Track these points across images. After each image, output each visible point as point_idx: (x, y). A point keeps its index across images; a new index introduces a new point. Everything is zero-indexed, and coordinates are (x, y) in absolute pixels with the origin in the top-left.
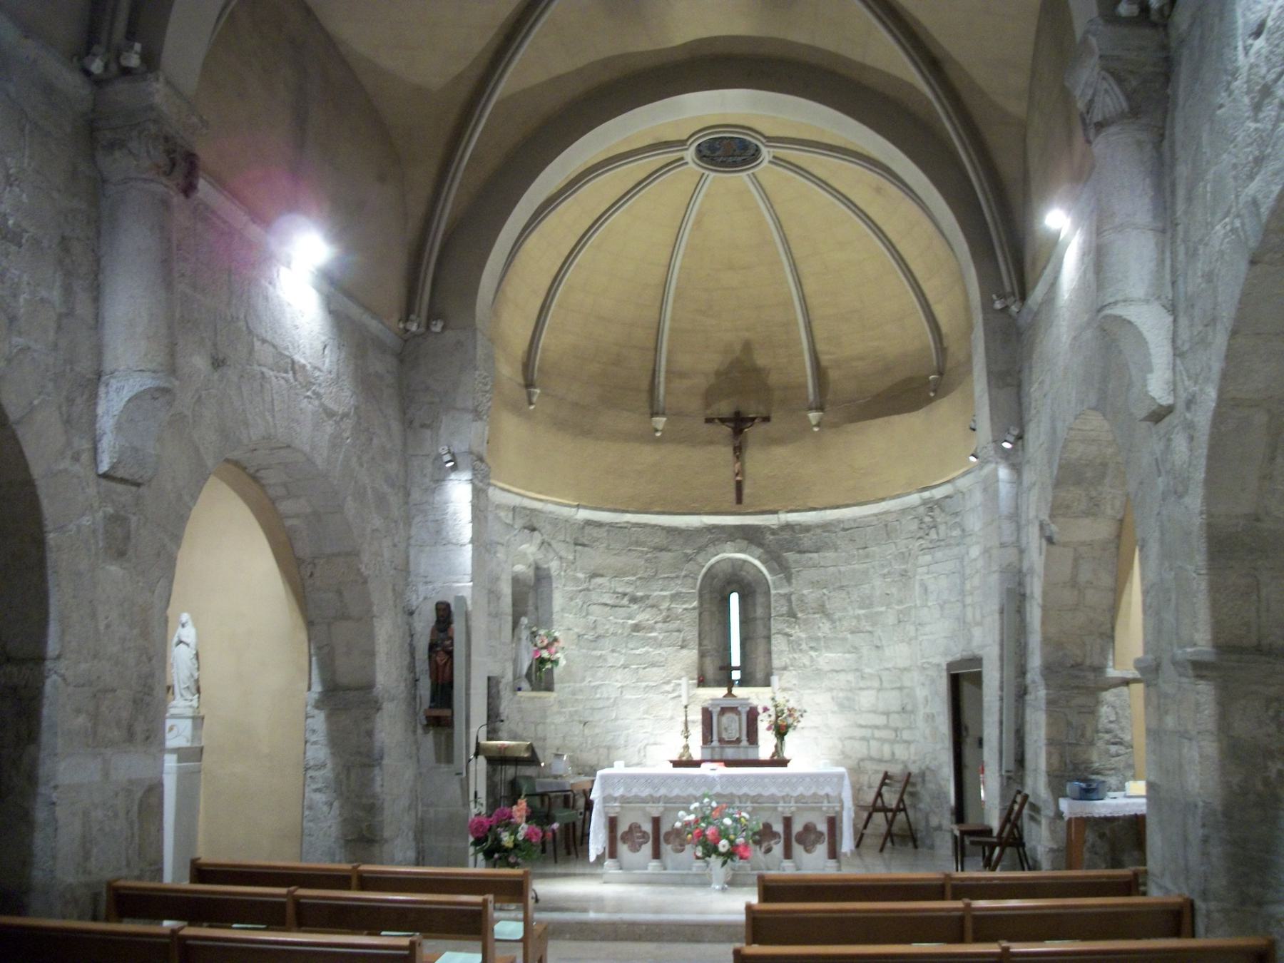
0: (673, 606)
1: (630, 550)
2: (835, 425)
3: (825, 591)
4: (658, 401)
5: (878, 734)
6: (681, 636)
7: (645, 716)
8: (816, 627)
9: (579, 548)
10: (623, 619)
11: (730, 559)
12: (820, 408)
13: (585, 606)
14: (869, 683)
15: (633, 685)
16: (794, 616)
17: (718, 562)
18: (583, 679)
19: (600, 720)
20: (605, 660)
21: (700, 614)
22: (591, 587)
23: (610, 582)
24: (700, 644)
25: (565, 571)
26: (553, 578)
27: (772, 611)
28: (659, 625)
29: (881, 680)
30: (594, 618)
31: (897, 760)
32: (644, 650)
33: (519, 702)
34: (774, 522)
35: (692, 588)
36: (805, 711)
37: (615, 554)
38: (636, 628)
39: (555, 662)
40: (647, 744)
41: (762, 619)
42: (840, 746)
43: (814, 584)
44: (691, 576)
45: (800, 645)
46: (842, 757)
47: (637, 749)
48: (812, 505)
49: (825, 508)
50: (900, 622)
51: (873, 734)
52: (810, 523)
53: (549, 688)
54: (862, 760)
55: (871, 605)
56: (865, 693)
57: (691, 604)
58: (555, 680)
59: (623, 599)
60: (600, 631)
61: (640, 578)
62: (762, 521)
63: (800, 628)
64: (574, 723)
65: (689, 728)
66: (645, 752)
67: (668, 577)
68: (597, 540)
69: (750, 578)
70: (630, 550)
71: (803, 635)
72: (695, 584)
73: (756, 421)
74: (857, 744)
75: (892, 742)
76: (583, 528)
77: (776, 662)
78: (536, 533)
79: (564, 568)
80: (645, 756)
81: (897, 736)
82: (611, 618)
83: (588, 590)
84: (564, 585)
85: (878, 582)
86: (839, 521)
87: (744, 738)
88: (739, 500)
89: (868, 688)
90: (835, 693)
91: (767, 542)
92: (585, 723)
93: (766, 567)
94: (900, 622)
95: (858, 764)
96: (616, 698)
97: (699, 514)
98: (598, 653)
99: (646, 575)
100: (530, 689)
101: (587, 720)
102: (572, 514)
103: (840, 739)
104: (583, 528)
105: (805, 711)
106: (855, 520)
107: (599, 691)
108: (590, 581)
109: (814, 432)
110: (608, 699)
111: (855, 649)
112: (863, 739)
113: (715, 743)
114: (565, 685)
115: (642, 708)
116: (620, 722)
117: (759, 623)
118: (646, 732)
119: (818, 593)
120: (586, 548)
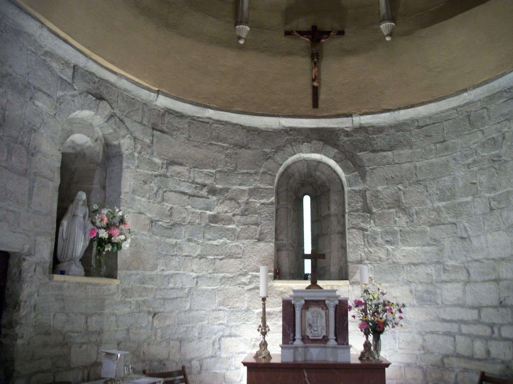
0: (250, 200)
1: (211, 144)
2: (408, 33)
3: (400, 186)
4: (243, 11)
5: (465, 329)
6: (259, 229)
7: (221, 307)
8: (392, 222)
9: (156, 133)
10: (201, 209)
11: (305, 160)
12: (393, 19)
13: (161, 192)
14: (453, 276)
15: (209, 276)
16: (370, 211)
17: (294, 163)
18: (155, 267)
19: (172, 311)
20: (181, 249)
21: (277, 210)
22: (168, 174)
23: (190, 172)
24: (276, 239)
25: (140, 153)
26: (124, 156)
27: (347, 206)
28: (238, 218)
29: (468, 272)
30: (171, 205)
31: (494, 359)
32: (221, 241)
33: (60, 288)
34: (348, 125)
35: (270, 185)
36: (404, 306)
37: (196, 146)
38: (214, 219)
39: (118, 246)
40: (222, 336)
41: (336, 215)
42: (421, 341)
43: (388, 180)
44: (269, 173)
45: (376, 239)
46: (422, 352)
47: (211, 341)
48: (385, 107)
49: (400, 109)
50: (492, 209)
51: (460, 330)
52: (382, 125)
53: (112, 274)
54: (447, 356)
55: (453, 196)
56: (449, 286)
57: (269, 199)
58: (119, 267)
59: (202, 189)
60: (176, 218)
61: (220, 172)
62: (337, 123)
63: (375, 222)
64: (142, 314)
65: (268, 323)
66: (220, 344)
67: (247, 173)
68: (178, 129)
69: (324, 177)
70: (211, 144)
71: (378, 230)
72: (273, 181)
73: (332, 33)
74: (440, 340)
75: (487, 339)
76: (163, 115)
77: (351, 256)
78: (104, 104)
79: (138, 149)
80: (220, 348)
81: (493, 332)
82: (189, 207)
83: (166, 176)
84: (138, 167)
85: (460, 173)
86: (413, 120)
87: (332, 336)
88: (315, 104)
89: (451, 281)
90: (413, 286)
91: (341, 143)
92: (155, 315)
93: (341, 166)
94: (492, 209)
95: (442, 360)
96: (191, 288)
97: (278, 116)
98: (173, 241)
99: (225, 169)
100: (83, 273)
101: (157, 310)
102: (152, 99)
103: (420, 333)
104: (163, 115)
105: (404, 306)
106: (430, 117)
107: (172, 280)
108: (167, 168)
109: (387, 41)
110: (182, 289)
111: (436, 242)
112: (447, 334)
113: (298, 342)
114: (133, 272)
115: (218, 299)
116: (194, 313)
117: (333, 219)
118: (221, 324)
119: (393, 189)
120: (165, 136)
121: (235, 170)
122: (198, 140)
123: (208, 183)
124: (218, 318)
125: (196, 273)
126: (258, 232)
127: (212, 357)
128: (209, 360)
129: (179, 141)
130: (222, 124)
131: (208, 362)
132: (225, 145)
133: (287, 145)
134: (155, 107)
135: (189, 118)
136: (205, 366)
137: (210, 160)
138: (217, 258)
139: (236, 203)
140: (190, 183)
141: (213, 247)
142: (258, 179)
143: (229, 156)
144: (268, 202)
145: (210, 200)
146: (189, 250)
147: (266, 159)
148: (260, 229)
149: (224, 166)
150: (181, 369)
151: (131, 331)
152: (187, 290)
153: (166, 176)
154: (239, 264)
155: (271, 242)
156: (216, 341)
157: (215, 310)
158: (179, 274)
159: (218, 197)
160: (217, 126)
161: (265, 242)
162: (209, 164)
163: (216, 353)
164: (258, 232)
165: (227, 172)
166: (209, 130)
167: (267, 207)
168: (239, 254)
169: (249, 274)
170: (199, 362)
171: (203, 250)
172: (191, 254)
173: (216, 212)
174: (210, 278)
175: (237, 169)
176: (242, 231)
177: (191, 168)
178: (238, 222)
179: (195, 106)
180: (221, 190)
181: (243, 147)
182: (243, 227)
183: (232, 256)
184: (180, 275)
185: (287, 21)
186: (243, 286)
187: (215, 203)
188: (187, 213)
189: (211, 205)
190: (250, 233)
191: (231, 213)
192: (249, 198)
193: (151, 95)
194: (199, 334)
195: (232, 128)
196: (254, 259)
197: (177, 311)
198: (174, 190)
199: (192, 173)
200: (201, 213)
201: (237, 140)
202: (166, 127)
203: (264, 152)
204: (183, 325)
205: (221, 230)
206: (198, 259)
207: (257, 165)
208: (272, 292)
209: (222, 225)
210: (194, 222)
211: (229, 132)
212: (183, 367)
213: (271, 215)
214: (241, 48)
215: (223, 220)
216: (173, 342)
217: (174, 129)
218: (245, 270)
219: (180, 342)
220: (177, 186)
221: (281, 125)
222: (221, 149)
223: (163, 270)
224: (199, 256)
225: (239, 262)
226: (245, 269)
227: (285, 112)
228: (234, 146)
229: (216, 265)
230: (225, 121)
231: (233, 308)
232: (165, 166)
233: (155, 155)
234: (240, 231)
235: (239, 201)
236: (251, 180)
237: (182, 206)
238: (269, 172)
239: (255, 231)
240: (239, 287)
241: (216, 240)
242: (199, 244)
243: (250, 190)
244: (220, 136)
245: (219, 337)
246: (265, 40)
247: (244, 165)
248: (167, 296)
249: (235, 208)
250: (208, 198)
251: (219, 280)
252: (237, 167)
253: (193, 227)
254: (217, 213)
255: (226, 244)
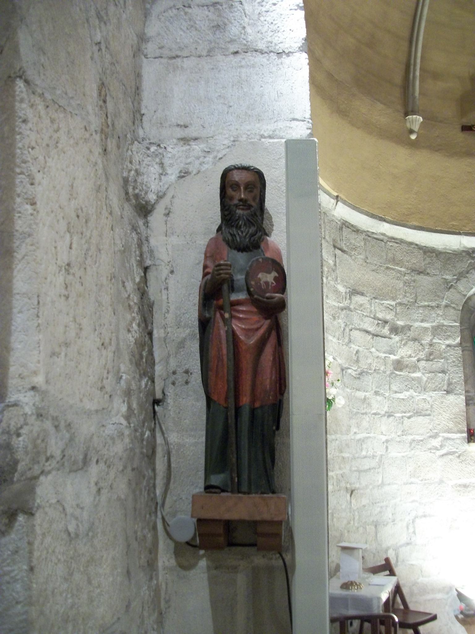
0: (434, 341)
1: (388, 268)
4: (414, 97)
6: (447, 378)
7: (413, 480)
10: (385, 353)
15: (398, 439)
19: (367, 486)
20: (369, 405)
22: (352, 307)
23: (371, 304)
30: (357, 348)
32: (407, 394)
38: (399, 365)
40: (416, 517)
60: (363, 365)
61: (400, 304)
66: (414, 527)
67: (428, 306)
70: (388, 268)
76: (341, 229)
80: (414, 532)
82: (373, 350)
83: (350, 310)
92: (352, 492)
97: (459, 234)
99: (405, 301)
101: (354, 486)
110: (374, 457)
116: (387, 488)
118: (413, 501)
121: (416, 302)
122: (375, 262)
123: (389, 318)
124: (410, 493)
125: (386, 435)
126: (445, 382)
127: (408, 544)
128: (404, 548)
129: (358, 263)
130: (397, 243)
131: (404, 552)
132: (403, 269)
133: (471, 271)
134: (333, 218)
135: (364, 234)
136: (401, 557)
137: (388, 288)
138: (405, 416)
139: (419, 344)
140: (372, 318)
141: (400, 401)
142: (441, 314)
143: (407, 284)
144: (454, 343)
145: (393, 341)
146: (377, 406)
147: (447, 287)
148: (447, 378)
149: (403, 298)
150: (384, 562)
151: (334, 515)
152: (378, 458)
153: (350, 310)
154: (429, 423)
155: (461, 395)
156: (409, 524)
157: (407, 484)
158: (370, 437)
159: (400, 336)
160: (392, 244)
161: (455, 394)
162: (388, 294)
163: (411, 539)
164: (445, 382)
165: (408, 305)
166: (384, 249)
167: (454, 349)
168: (427, 410)
169: (439, 436)
170: (394, 552)
171: (390, 406)
172: (379, 411)
173: (400, 356)
174: (399, 442)
175: (417, 301)
176: (429, 380)
177: (372, 299)
178: (424, 369)
179: (370, 219)
180: (403, 327)
181: (421, 272)
182: (430, 375)
183: (420, 412)
184: (371, 439)
185: (463, 112)
186: (435, 451)
187: (398, 345)
188: (372, 358)
189: (394, 347)
190: (437, 384)
191: (415, 357)
192: (433, 338)
193: (330, 202)
194: (393, 514)
195: (407, 248)
196: (444, 416)
197: (371, 487)
198: (358, 328)
199: (373, 305)
200: (385, 357)
201: (414, 263)
202: (345, 244)
203: (445, 279)
204: (377, 504)
205: (407, 379)
206: (386, 417)
207: (438, 296)
208: (467, 459)
209: (407, 373)
210: (379, 370)
211: (405, 253)
212: (387, 560)
213: (458, 360)
214: (414, 145)
215: (407, 366)
216: (370, 526)
217: (352, 248)
218: (435, 431)
219: (376, 526)
220: (361, 323)
221: (462, 246)
222: (399, 275)
223: (355, 433)
224: (387, 414)
225: (428, 421)
226: (435, 429)
227: (467, 229)
228: (412, 272)
229: (404, 425)
230: (399, 239)
231: (425, 480)
232: (348, 297)
233: (339, 281)
234: (427, 381)
235: (423, 342)
236: (433, 315)
237: (367, 349)
238: (452, 305)
239: (442, 381)
240: (431, 452)
241: (402, 393)
242: (385, 398)
243: (433, 327)
244: (395, 257)
245: (413, 518)
246: (438, 136)
247: (424, 296)
248: (361, 468)
249: (419, 350)
250: (390, 338)
251: (408, 445)
252: (417, 298)
253: (379, 376)
254: (401, 358)
255: (413, 397)
